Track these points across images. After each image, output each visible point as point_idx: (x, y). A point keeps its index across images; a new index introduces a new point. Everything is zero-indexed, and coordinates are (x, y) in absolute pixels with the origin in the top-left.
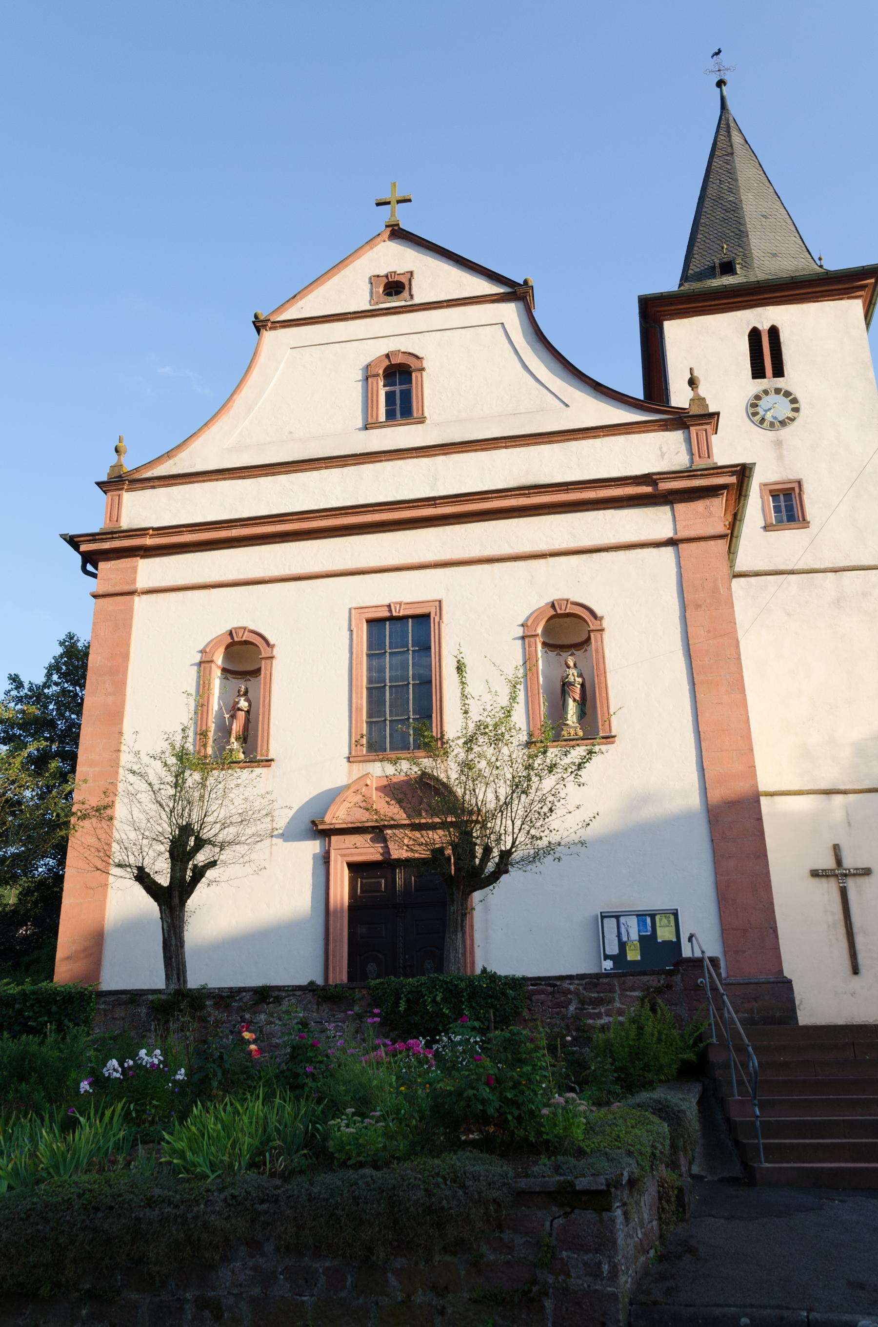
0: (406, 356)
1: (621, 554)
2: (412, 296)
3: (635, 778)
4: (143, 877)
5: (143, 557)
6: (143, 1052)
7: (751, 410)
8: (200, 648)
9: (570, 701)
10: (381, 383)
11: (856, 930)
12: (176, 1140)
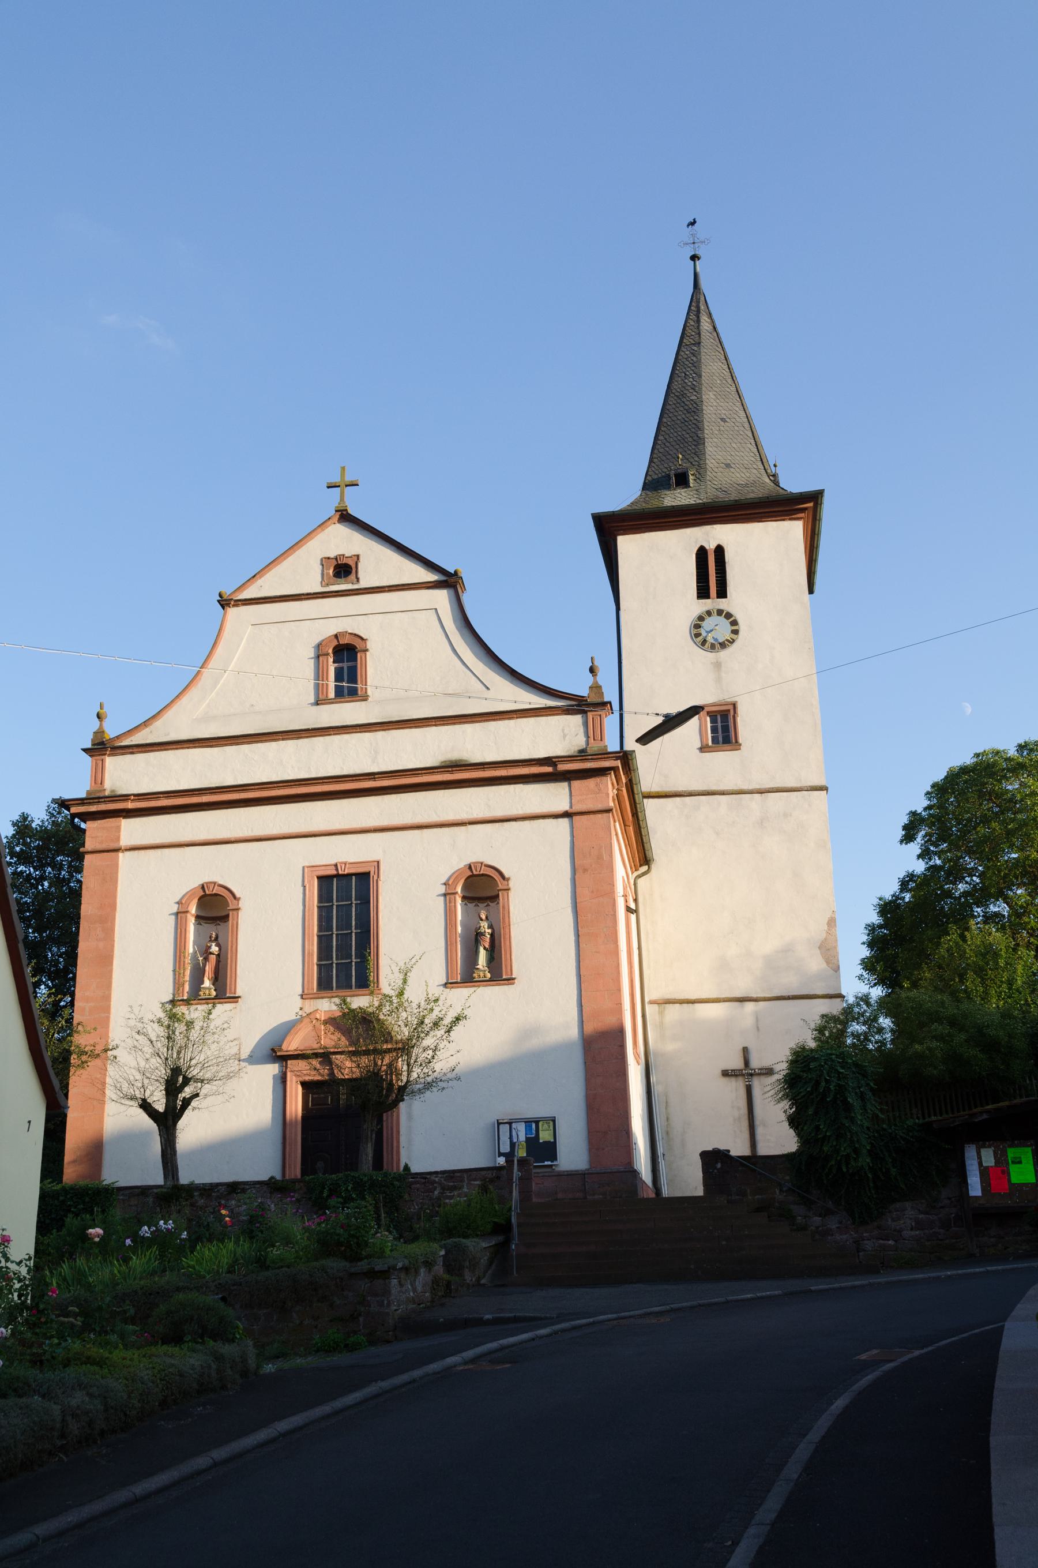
0: (352, 637)
1: (527, 823)
2: (358, 579)
3: (531, 1010)
4: (145, 1106)
5: (125, 817)
6: (161, 1222)
7: (695, 631)
8: (177, 900)
9: (481, 949)
10: (331, 660)
11: (757, 1122)
12: (189, 1261)
